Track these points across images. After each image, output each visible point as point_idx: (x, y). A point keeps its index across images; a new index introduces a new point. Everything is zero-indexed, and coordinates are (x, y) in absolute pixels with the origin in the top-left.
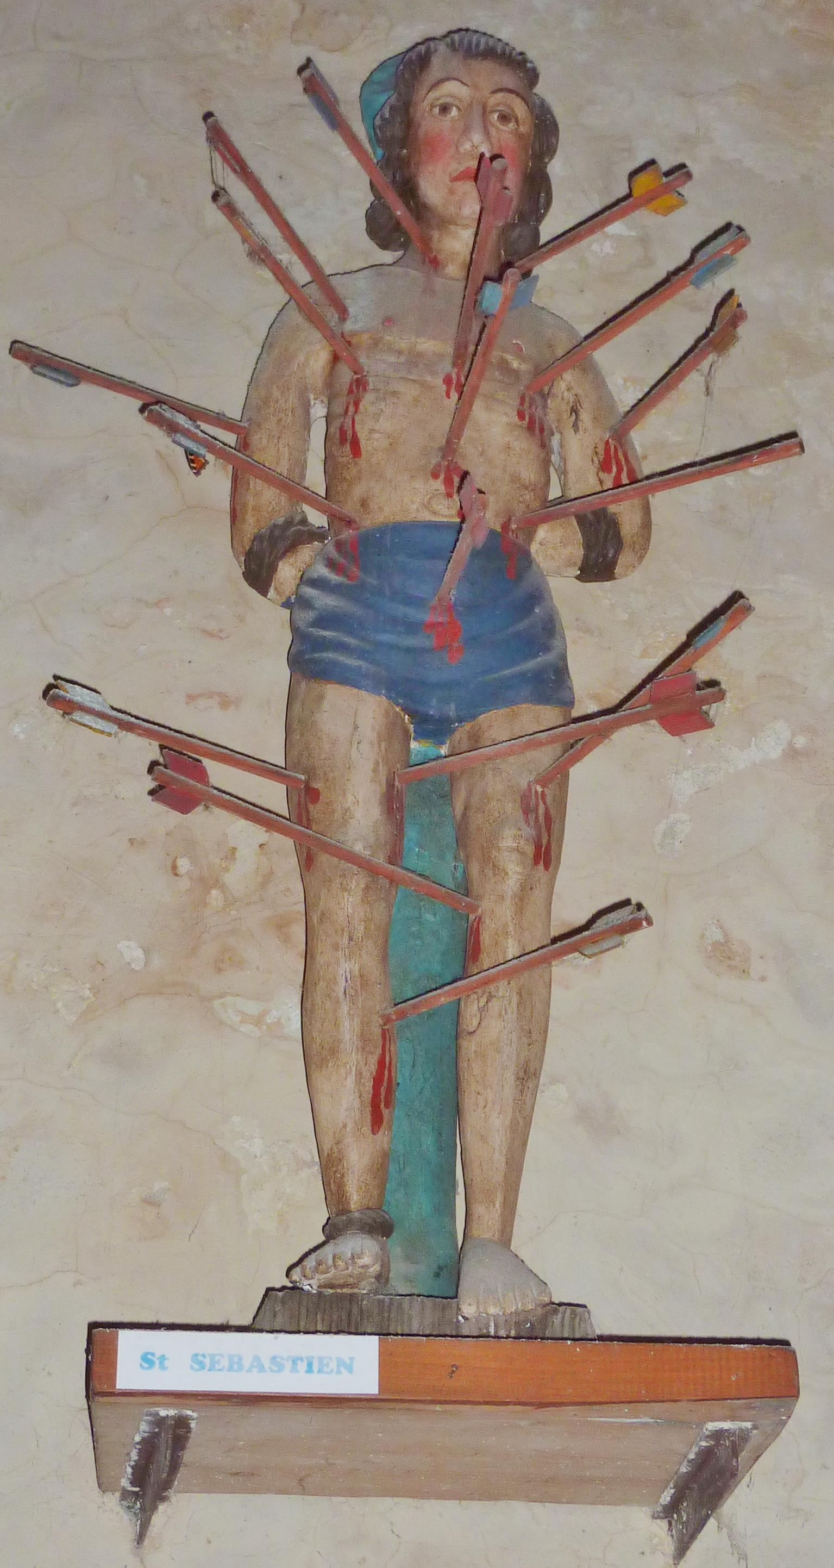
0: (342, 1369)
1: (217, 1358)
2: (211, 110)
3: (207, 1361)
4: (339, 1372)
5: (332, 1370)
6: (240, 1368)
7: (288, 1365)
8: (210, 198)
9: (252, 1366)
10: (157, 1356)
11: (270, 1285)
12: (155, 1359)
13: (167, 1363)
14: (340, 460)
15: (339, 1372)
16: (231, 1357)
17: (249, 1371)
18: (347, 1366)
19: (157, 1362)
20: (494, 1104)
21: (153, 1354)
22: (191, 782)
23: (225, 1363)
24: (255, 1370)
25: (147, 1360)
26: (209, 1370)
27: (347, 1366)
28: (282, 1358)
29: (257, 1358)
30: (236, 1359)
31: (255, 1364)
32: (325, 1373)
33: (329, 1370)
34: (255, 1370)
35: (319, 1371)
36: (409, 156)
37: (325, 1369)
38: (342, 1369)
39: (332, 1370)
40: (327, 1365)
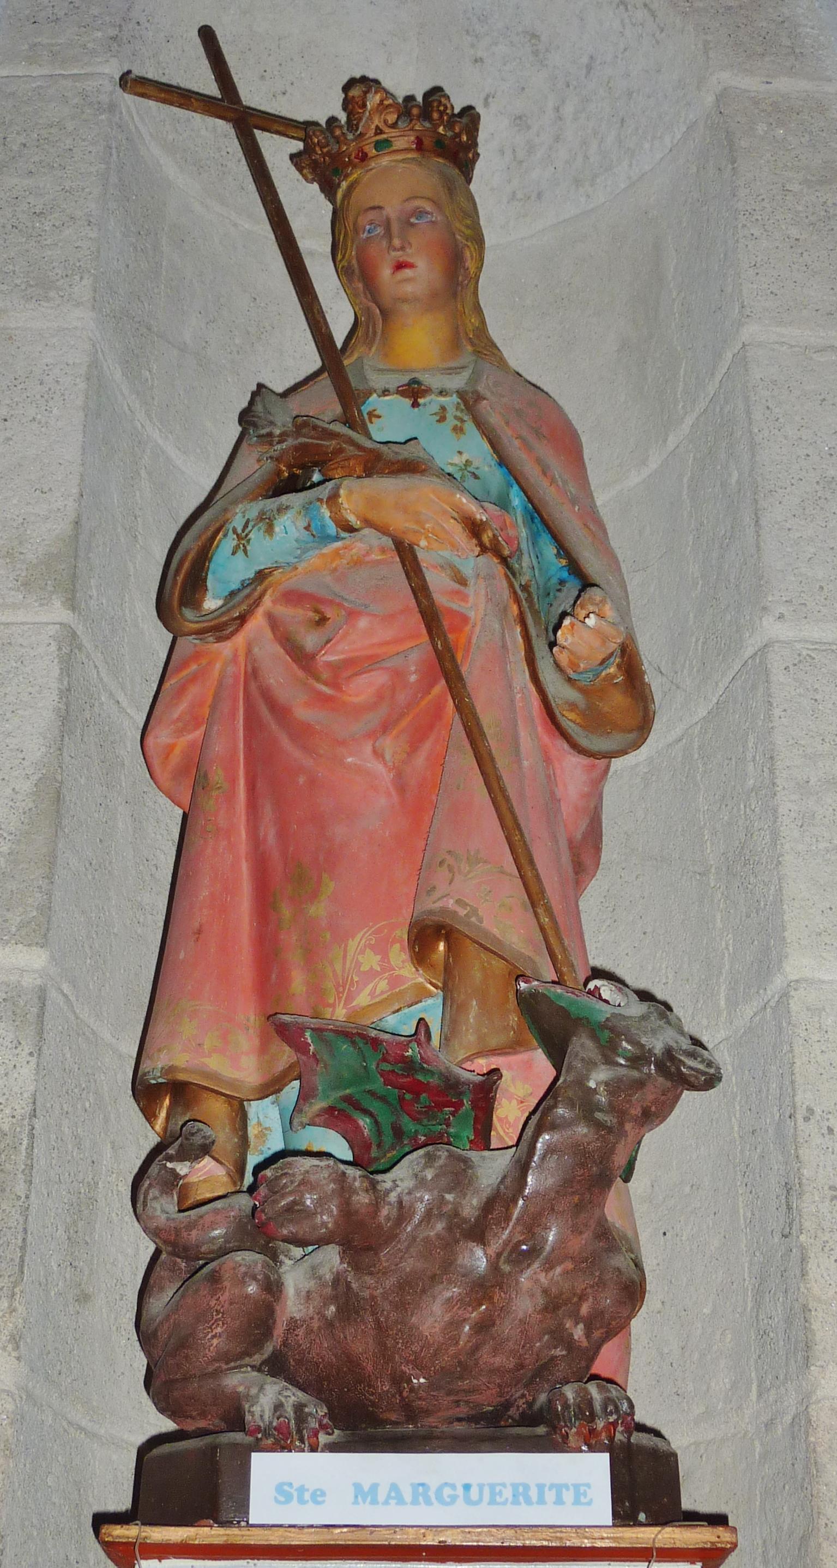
1: (582, 1489)
2: (330, 114)
5: (507, 1499)
8: (202, 24)
9: (389, 1497)
10: (296, 1486)
12: (292, 1491)
16: (515, 1486)
17: (386, 1503)
18: (580, 1494)
19: (295, 1494)
21: (290, 1485)
22: (241, 746)
23: (508, 1493)
24: (393, 1502)
26: (489, 1504)
29: (394, 1487)
30: (521, 1489)
32: (499, 1504)
33: (503, 1500)
34: (393, 1502)
39: (507, 1499)
40: (500, 1493)
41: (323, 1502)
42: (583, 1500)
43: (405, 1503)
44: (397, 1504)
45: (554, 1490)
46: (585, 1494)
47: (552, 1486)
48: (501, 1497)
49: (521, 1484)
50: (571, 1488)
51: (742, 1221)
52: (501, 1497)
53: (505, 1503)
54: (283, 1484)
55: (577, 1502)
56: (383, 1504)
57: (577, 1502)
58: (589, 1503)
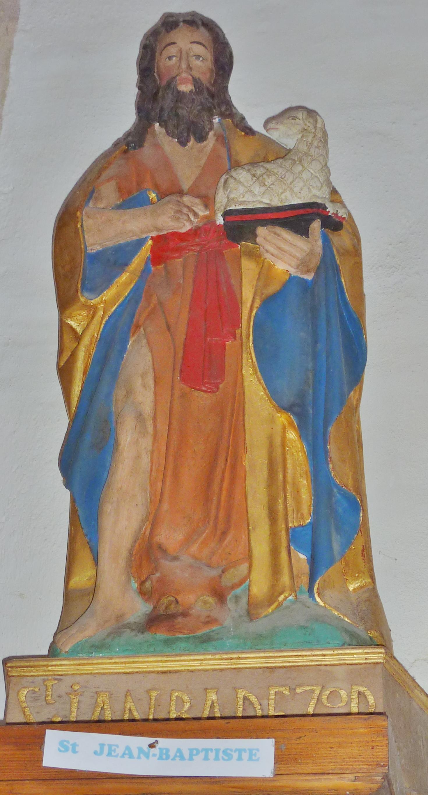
0: (142, 755)
1: (254, 752)
3: (221, 754)
4: (139, 758)
5: (118, 754)
6: (168, 758)
7: (235, 755)
9: (176, 756)
11: (7, 655)
12: (69, 745)
13: (77, 749)
14: (263, 393)
15: (139, 758)
18: (64, 747)
19: (71, 747)
20: (214, 232)
25: (252, 755)
27: (252, 755)
28: (231, 750)
29: (179, 750)
30: (164, 751)
31: (127, 752)
33: (115, 754)
34: (127, 756)
35: (109, 754)
36: (151, 203)
37: (113, 753)
38: (142, 755)
39: (118, 754)
41: (259, 758)
42: (254, 758)
43: (134, 758)
44: (180, 760)
45: (237, 752)
46: (255, 755)
47: (236, 750)
48: (115, 752)
49: (164, 749)
50: (248, 751)
51: (191, 635)
52: (115, 752)
53: (117, 756)
54: (227, 749)
55: (250, 759)
56: (120, 757)
57: (250, 759)
58: (258, 760)
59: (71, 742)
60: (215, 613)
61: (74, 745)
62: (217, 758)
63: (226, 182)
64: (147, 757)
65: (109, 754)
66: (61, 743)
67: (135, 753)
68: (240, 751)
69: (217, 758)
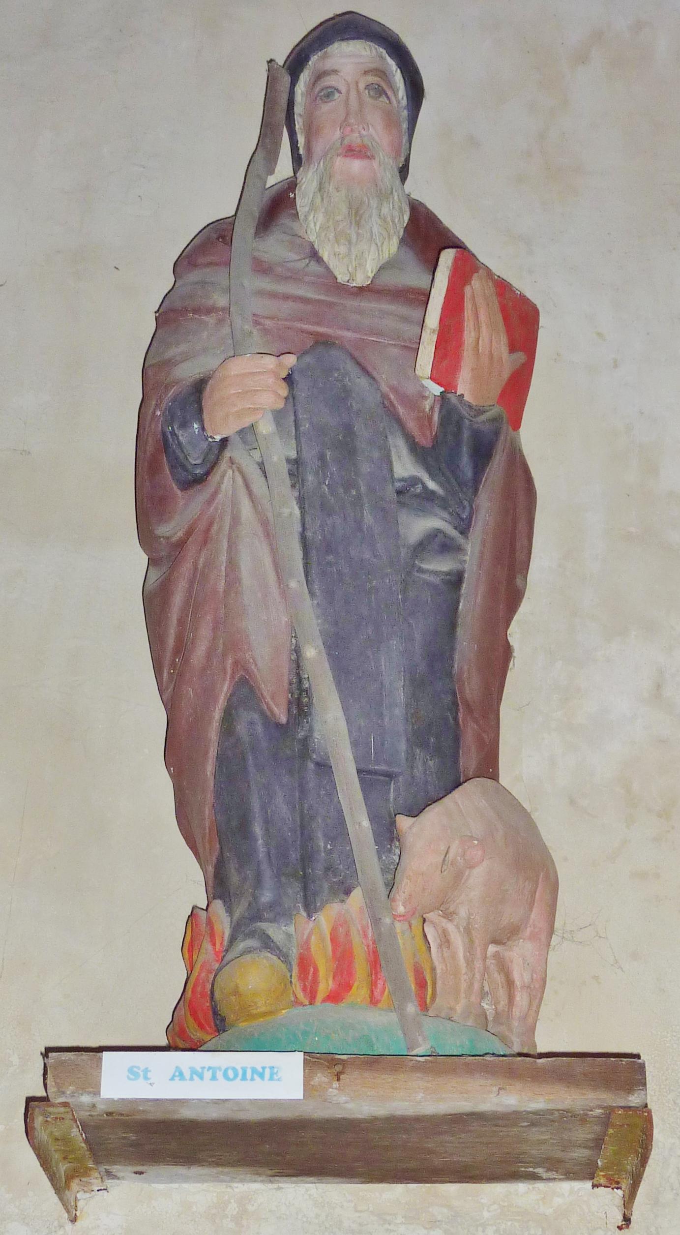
0: (194, 1076)
7: (208, 1075)
13: (149, 1075)
15: (192, 1079)
18: (133, 1073)
19: (142, 1074)
35: (271, 1079)
38: (194, 1076)
47: (210, 1068)
54: (133, 1067)
59: (142, 1068)
60: (320, 996)
61: (146, 1071)
62: (214, 1078)
63: (292, 694)
64: (202, 1078)
65: (271, 1079)
66: (131, 1070)
67: (187, 1074)
68: (213, 1070)
69: (244, 1078)
